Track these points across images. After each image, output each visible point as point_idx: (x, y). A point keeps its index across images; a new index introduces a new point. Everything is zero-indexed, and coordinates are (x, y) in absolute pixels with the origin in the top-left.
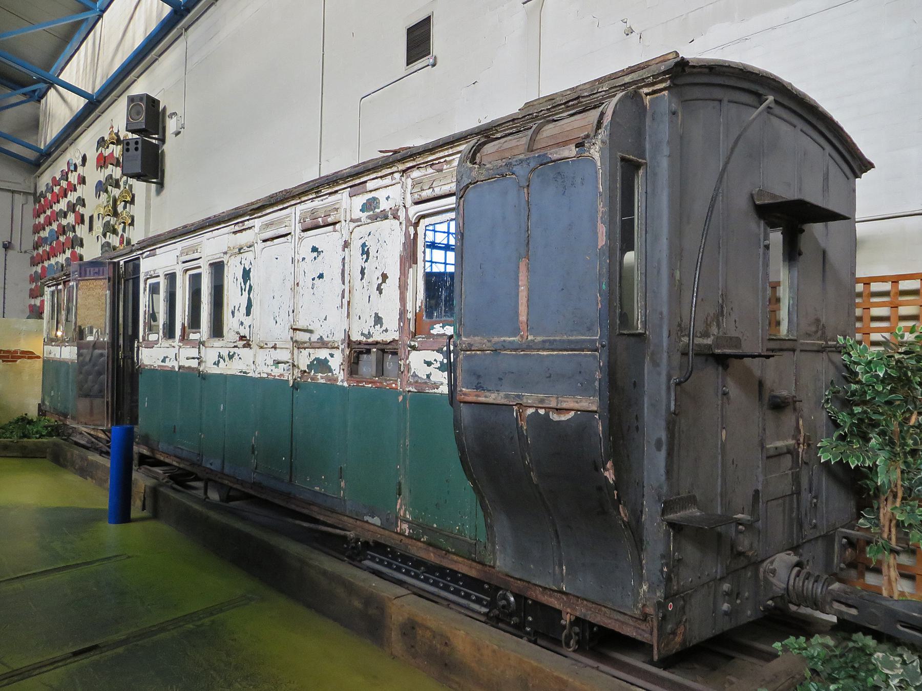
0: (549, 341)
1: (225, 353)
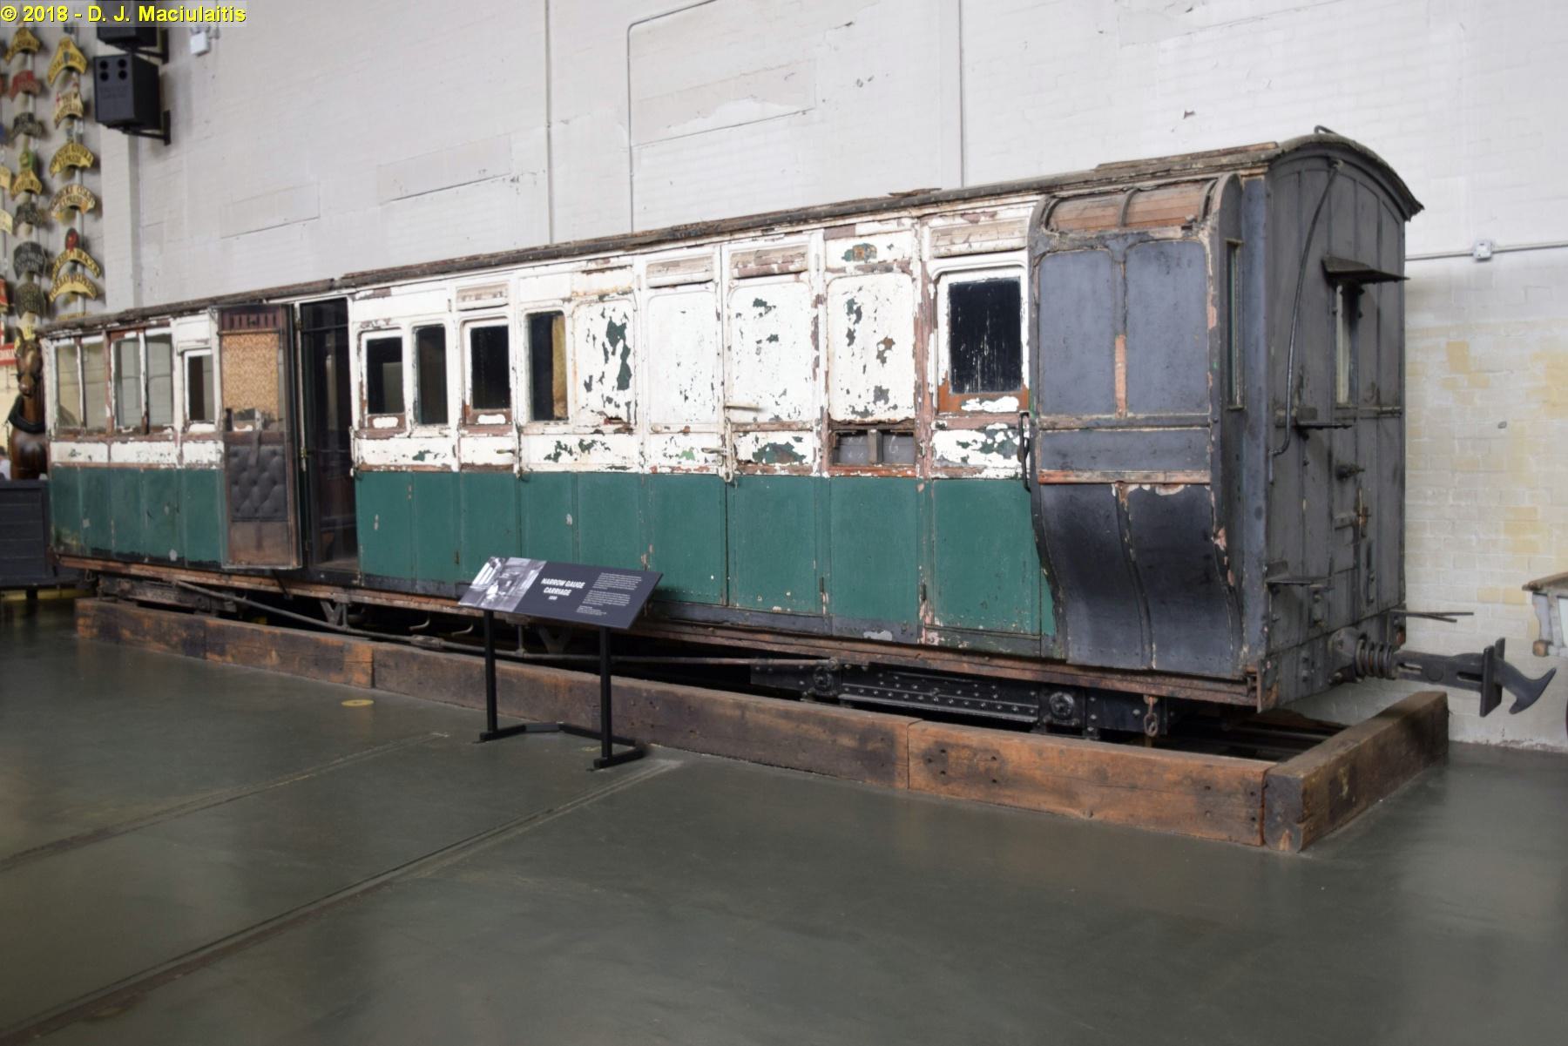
0: (1154, 418)
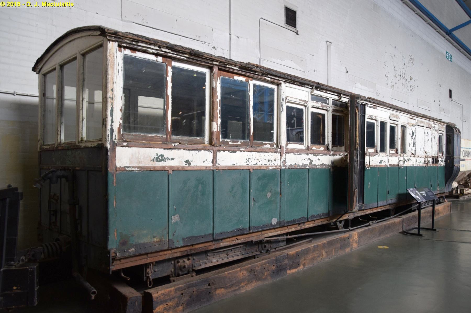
1: (406, 159)
